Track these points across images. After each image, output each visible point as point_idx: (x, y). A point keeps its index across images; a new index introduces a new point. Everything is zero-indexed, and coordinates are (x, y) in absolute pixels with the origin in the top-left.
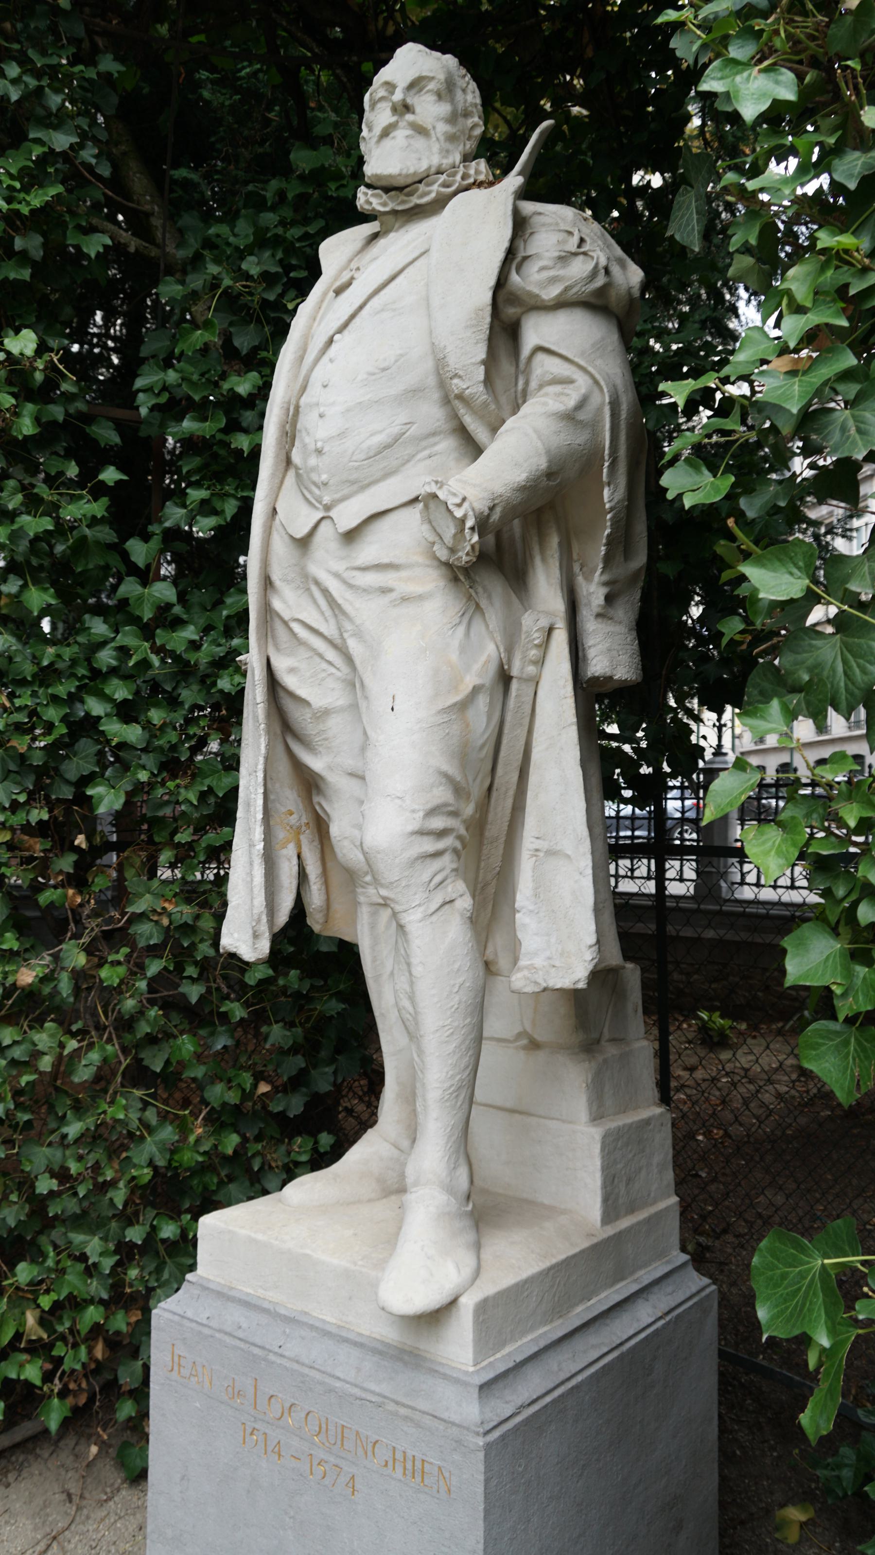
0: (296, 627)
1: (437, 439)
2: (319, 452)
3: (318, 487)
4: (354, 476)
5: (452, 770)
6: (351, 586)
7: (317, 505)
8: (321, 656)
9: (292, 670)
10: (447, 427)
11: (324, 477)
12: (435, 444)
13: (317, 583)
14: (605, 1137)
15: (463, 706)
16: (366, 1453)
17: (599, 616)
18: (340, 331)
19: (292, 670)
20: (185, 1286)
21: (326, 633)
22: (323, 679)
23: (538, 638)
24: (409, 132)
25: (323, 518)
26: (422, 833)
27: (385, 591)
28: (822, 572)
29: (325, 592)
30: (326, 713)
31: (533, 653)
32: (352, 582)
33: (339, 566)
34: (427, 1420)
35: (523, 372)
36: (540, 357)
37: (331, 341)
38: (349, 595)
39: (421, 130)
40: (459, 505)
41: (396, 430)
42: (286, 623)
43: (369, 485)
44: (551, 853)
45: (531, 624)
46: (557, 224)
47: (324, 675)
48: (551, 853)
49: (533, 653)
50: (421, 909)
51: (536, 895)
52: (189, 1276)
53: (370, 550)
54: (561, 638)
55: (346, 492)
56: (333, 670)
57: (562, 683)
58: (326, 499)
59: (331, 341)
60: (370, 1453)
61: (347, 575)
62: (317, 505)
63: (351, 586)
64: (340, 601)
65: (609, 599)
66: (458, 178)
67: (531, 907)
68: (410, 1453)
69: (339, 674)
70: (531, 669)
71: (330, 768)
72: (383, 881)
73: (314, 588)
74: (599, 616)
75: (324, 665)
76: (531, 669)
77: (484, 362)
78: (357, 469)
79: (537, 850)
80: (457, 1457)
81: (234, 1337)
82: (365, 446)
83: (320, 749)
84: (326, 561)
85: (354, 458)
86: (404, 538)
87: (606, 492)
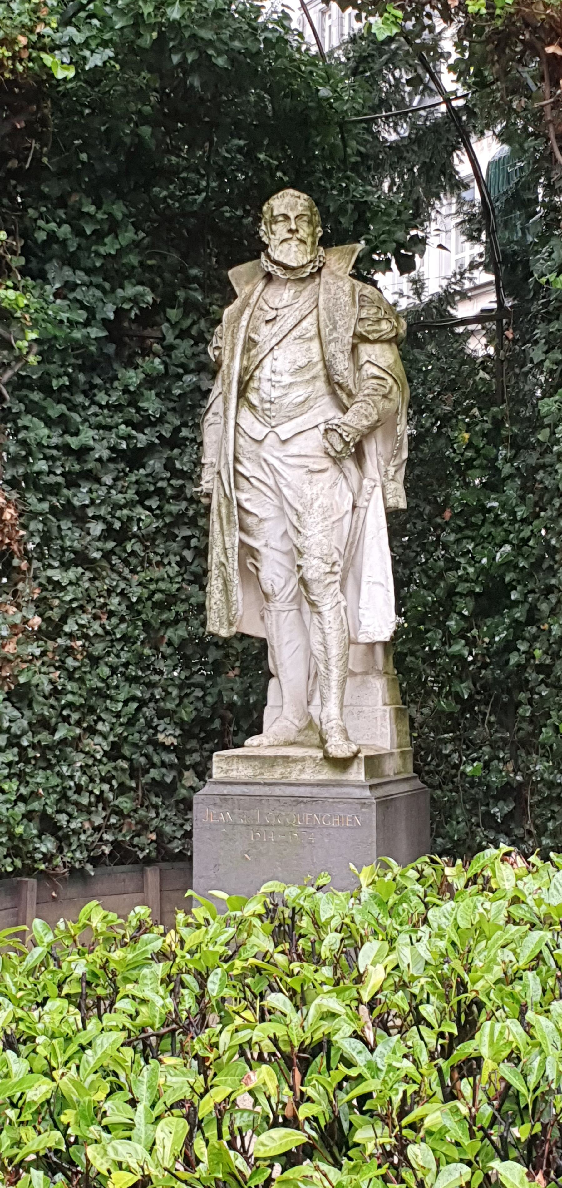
0: (252, 480)
2: (272, 403)
8: (265, 494)
9: (247, 500)
11: (274, 414)
13: (265, 460)
19: (247, 500)
24: (297, 243)
28: (200, 298)
33: (280, 455)
37: (272, 349)
38: (284, 467)
39: (302, 241)
42: (247, 479)
53: (293, 448)
54: (378, 490)
58: (273, 424)
59: (272, 349)
61: (283, 459)
73: (264, 464)
75: (265, 498)
76: (366, 504)
81: (259, 784)
84: (270, 452)
86: (312, 443)
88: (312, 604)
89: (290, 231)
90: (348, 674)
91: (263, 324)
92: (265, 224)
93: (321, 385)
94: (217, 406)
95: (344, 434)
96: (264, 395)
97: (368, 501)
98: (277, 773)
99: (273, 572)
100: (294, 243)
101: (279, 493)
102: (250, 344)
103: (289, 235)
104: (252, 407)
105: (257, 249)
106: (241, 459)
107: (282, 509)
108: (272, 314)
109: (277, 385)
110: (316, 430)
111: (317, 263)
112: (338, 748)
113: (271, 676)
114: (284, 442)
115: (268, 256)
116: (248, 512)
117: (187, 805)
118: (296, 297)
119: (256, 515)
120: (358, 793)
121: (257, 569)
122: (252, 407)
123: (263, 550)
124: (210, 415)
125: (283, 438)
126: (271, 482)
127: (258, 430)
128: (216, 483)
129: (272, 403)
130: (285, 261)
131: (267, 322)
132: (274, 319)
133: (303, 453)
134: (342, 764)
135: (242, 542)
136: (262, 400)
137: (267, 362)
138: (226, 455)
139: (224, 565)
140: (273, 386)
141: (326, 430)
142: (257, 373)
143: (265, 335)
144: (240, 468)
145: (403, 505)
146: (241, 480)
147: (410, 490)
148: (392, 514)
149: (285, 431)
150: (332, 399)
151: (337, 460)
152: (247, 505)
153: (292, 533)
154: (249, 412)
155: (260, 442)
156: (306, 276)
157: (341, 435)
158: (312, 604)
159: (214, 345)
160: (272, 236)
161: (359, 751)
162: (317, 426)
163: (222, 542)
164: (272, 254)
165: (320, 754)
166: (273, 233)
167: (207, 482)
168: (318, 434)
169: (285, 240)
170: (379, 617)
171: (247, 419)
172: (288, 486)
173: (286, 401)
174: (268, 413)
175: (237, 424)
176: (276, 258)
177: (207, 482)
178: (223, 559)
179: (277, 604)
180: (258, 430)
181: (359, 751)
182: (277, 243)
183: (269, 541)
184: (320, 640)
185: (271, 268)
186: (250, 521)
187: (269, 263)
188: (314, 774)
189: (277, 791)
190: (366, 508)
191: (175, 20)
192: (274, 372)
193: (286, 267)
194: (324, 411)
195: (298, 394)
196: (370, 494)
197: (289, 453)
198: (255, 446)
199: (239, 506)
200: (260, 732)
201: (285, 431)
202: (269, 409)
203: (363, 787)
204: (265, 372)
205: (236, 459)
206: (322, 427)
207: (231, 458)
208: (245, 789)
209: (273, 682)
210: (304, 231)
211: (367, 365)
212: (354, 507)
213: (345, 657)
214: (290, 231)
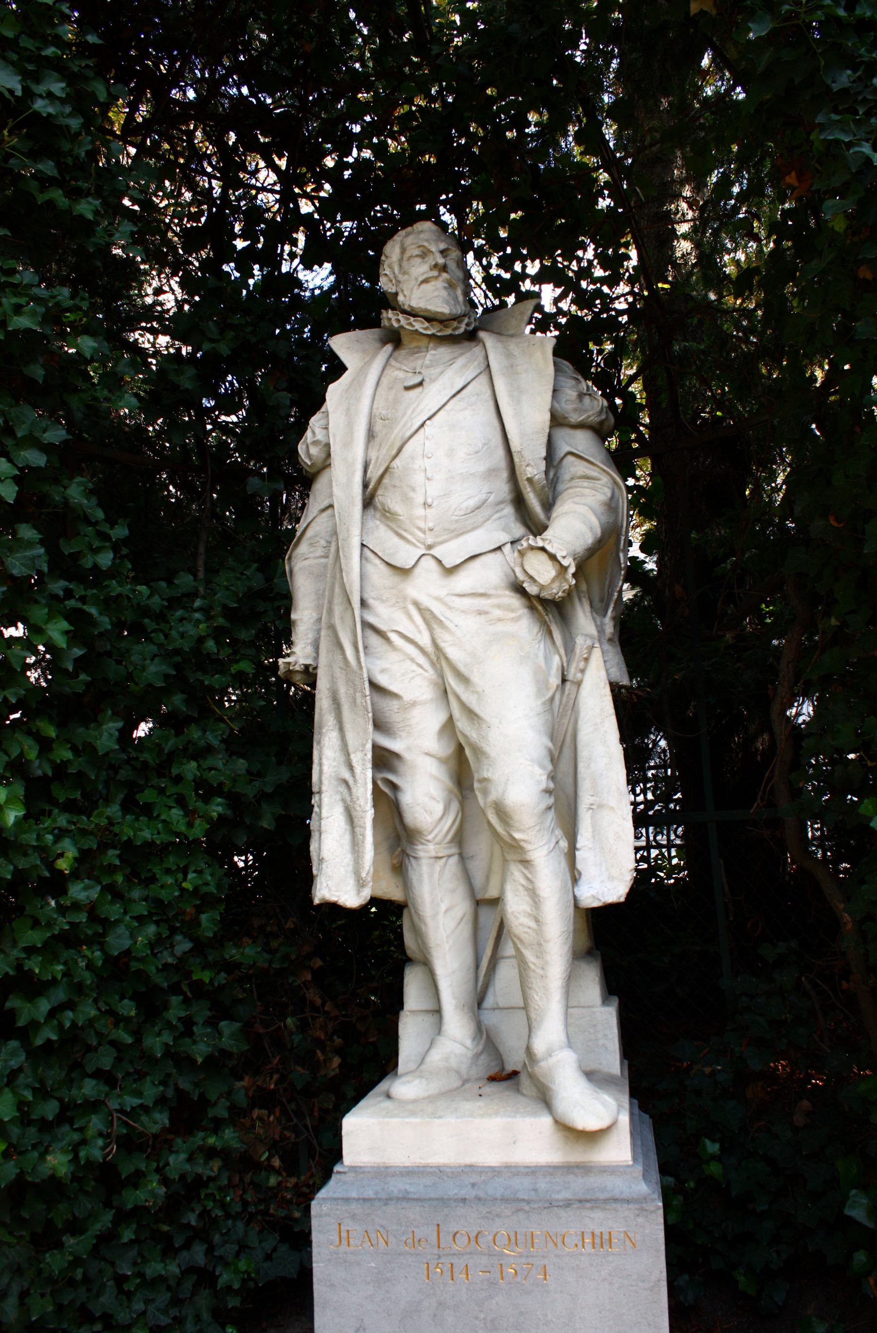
0: (393, 637)
1: (502, 506)
3: (424, 533)
4: (452, 527)
7: (418, 544)
8: (412, 660)
9: (383, 671)
10: (509, 497)
12: (503, 509)
15: (552, 699)
16: (556, 1245)
18: (429, 419)
20: (334, 1177)
21: (421, 643)
22: (412, 678)
25: (423, 555)
30: (414, 704)
31: (582, 664)
32: (452, 605)
33: (442, 593)
35: (554, 467)
36: (570, 458)
37: (422, 425)
38: (448, 613)
43: (462, 534)
47: (413, 674)
50: (547, 847)
51: (594, 836)
52: (337, 1168)
53: (465, 580)
55: (444, 537)
56: (420, 671)
58: (430, 541)
59: (422, 425)
60: (559, 1244)
62: (418, 544)
64: (442, 618)
67: (590, 846)
68: (597, 1232)
69: (426, 674)
70: (579, 675)
71: (409, 749)
72: (522, 828)
75: (415, 667)
77: (545, 459)
78: (456, 521)
79: (592, 804)
80: (640, 1220)
83: (401, 733)
85: (456, 513)
97: (583, 671)
103: (435, 273)
113: (409, 960)
121: (395, 787)
125: (448, 565)
126: (425, 640)
131: (407, 388)
139: (345, 782)
152: (383, 680)
154: (382, 529)
156: (462, 331)
162: (499, 548)
178: (347, 775)
179: (431, 847)
186: (390, 707)
190: (579, 684)
191: (286, 1018)
193: (430, 318)
196: (587, 660)
197: (458, 590)
205: (363, 603)
207: (356, 604)
212: (564, 680)
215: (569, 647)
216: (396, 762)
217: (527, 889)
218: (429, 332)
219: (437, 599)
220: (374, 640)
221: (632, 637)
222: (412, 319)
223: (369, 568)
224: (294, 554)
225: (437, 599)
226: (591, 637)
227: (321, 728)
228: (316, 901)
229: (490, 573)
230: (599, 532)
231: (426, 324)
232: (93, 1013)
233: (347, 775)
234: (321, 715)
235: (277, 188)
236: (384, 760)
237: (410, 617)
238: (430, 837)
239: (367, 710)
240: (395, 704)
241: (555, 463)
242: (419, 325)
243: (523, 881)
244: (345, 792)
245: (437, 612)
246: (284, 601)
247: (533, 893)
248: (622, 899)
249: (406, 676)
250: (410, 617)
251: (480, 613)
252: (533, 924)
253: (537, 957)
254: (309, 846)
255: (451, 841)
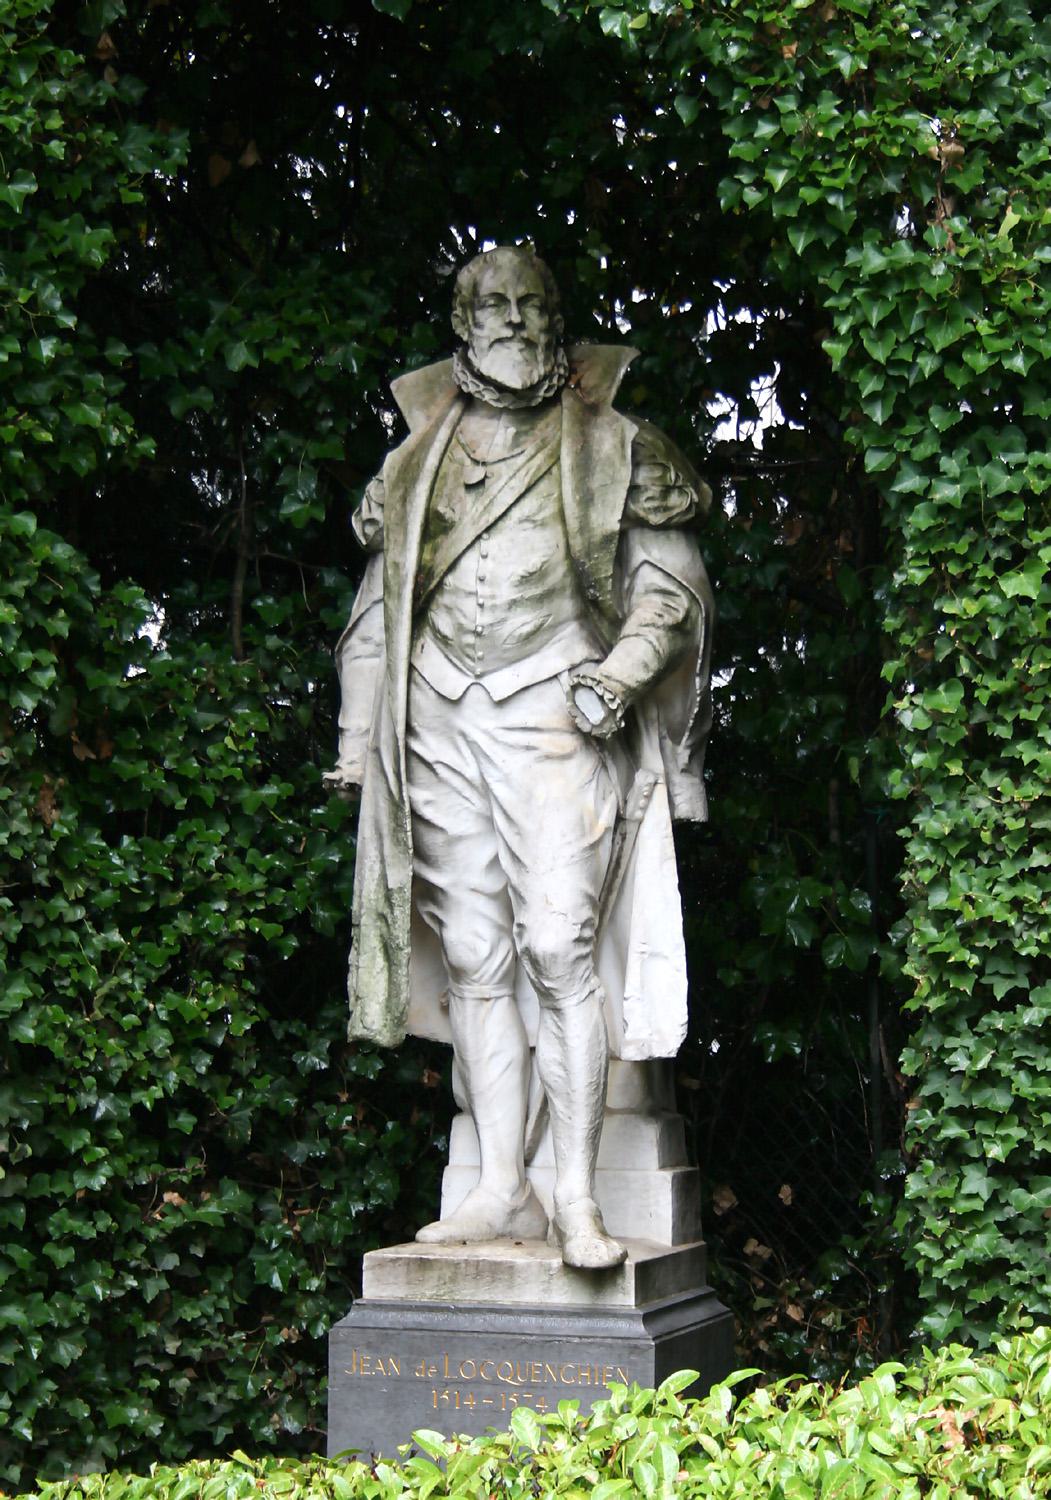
0: (439, 769)
2: (478, 635)
5: (591, 891)
6: (495, 740)
8: (459, 793)
9: (428, 803)
13: (463, 735)
14: (674, 1178)
15: (594, 846)
17: (683, 771)
19: (428, 803)
23: (646, 791)
26: (579, 940)
27: (529, 748)
29: (471, 744)
30: (459, 838)
31: (642, 802)
34: (609, 1341)
40: (613, 700)
41: (538, 622)
42: (428, 765)
44: (653, 955)
45: (641, 779)
46: (654, 456)
48: (653, 955)
49: (642, 802)
53: (517, 714)
54: (661, 793)
57: (664, 825)
58: (479, 671)
63: (495, 740)
65: (691, 757)
66: (555, 381)
71: (455, 885)
74: (683, 771)
76: (638, 814)
82: (517, 633)
84: (477, 719)
87: (697, 680)
88: (545, 994)
89: (510, 324)
90: (602, 1110)
91: (462, 491)
92: (463, 305)
93: (567, 606)
94: (372, 625)
95: (608, 696)
96: (463, 620)
97: (644, 809)
98: (470, 1293)
99: (469, 932)
100: (515, 346)
101: (485, 790)
102: (436, 526)
103: (508, 333)
104: (443, 640)
105: (448, 344)
106: (418, 729)
107: (490, 820)
108: (477, 474)
109: (488, 603)
110: (555, 683)
111: (555, 381)
112: (592, 1251)
113: (459, 1111)
114: (501, 704)
115: (467, 363)
116: (428, 823)
117: (315, 1353)
118: (517, 440)
119: (442, 830)
120: (623, 1327)
121: (440, 923)
122: (443, 640)
123: (452, 891)
124: (354, 641)
126: (471, 772)
127: (453, 682)
128: (370, 770)
129: (478, 635)
130: (499, 379)
131: (469, 487)
132: (481, 483)
133: (531, 724)
134: (600, 1278)
135: (417, 879)
136: (461, 629)
137: (470, 563)
138: (394, 723)
140: (481, 606)
141: (575, 688)
142: (449, 580)
143: (469, 514)
144: (416, 746)
145: (700, 816)
146: (415, 763)
147: (713, 790)
148: (682, 830)
149: (502, 682)
150: (582, 626)
151: (591, 740)
152: (427, 812)
153: (505, 861)
155: (456, 703)
157: (601, 698)
158: (545, 994)
159: (365, 515)
160: (476, 331)
161: (625, 1256)
162: (556, 676)
163: (377, 870)
164: (475, 362)
165: (557, 1262)
166: (478, 325)
167: (352, 763)
168: (557, 692)
169: (500, 341)
170: (657, 1012)
171: (433, 662)
172: (506, 780)
173: (506, 630)
174: (470, 652)
175: (411, 668)
176: (485, 371)
177: (352, 763)
178: (386, 911)
180: (453, 682)
181: (625, 1256)
182: (485, 343)
183: (463, 876)
184: (558, 1057)
185: (472, 386)
186: (432, 840)
187: (470, 378)
188: (565, 1294)
189: (480, 1322)
190: (640, 822)
192: (482, 580)
193: (501, 388)
194: (567, 647)
195: (523, 621)
196: (649, 797)
198: (444, 708)
199: (416, 816)
200: (437, 1218)
201: (502, 682)
202: (472, 646)
203: (629, 1316)
204: (466, 576)
205: (410, 730)
206: (566, 681)
207: (401, 729)
208: (420, 1318)
209: (460, 1127)
210: (535, 321)
211: (646, 569)
213: (602, 1089)
214: (510, 324)
215: (628, 783)
216: (441, 897)
217: (557, 1037)
218: (500, 405)
219: (486, 732)
220: (421, 772)
221: (720, 759)
222: (482, 386)
223: (417, 695)
224: (345, 647)
225: (486, 732)
226: (656, 775)
227: (362, 858)
228: (350, 1040)
229: (546, 708)
230: (654, 665)
231: (496, 396)
232: (77, 1186)
233: (386, 911)
234: (363, 843)
235: (308, 404)
236: (425, 892)
237: (458, 749)
238: (476, 977)
239: (406, 844)
240: (439, 838)
241: (631, 571)
242: (489, 396)
243: (555, 1030)
244: (385, 929)
245: (485, 748)
246: (331, 696)
247: (562, 1041)
248: (673, 1055)
249: (446, 809)
250: (458, 749)
251: (529, 748)
252: (561, 1073)
253: (567, 1107)
254: (346, 980)
255: (501, 981)
